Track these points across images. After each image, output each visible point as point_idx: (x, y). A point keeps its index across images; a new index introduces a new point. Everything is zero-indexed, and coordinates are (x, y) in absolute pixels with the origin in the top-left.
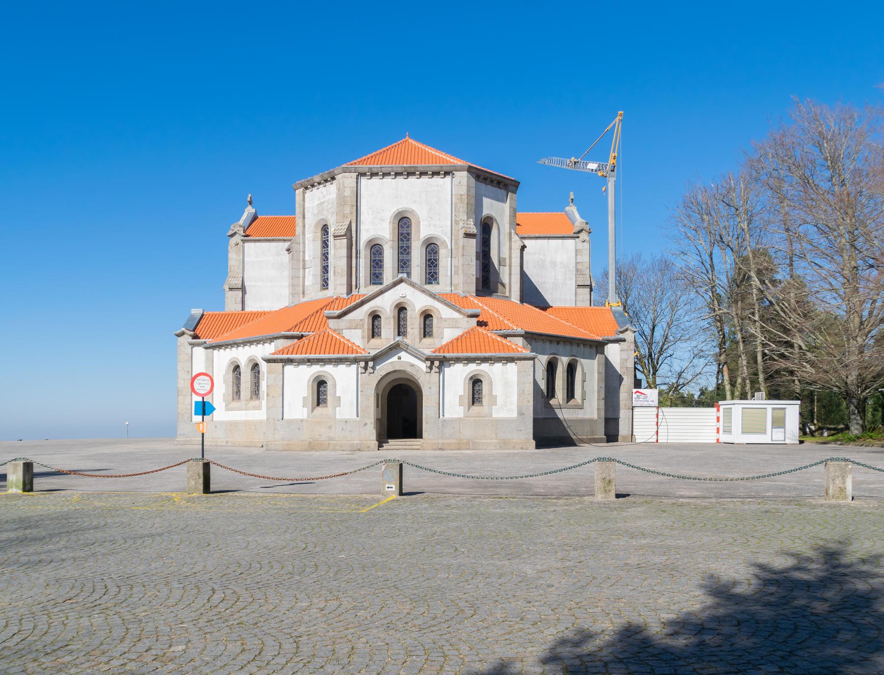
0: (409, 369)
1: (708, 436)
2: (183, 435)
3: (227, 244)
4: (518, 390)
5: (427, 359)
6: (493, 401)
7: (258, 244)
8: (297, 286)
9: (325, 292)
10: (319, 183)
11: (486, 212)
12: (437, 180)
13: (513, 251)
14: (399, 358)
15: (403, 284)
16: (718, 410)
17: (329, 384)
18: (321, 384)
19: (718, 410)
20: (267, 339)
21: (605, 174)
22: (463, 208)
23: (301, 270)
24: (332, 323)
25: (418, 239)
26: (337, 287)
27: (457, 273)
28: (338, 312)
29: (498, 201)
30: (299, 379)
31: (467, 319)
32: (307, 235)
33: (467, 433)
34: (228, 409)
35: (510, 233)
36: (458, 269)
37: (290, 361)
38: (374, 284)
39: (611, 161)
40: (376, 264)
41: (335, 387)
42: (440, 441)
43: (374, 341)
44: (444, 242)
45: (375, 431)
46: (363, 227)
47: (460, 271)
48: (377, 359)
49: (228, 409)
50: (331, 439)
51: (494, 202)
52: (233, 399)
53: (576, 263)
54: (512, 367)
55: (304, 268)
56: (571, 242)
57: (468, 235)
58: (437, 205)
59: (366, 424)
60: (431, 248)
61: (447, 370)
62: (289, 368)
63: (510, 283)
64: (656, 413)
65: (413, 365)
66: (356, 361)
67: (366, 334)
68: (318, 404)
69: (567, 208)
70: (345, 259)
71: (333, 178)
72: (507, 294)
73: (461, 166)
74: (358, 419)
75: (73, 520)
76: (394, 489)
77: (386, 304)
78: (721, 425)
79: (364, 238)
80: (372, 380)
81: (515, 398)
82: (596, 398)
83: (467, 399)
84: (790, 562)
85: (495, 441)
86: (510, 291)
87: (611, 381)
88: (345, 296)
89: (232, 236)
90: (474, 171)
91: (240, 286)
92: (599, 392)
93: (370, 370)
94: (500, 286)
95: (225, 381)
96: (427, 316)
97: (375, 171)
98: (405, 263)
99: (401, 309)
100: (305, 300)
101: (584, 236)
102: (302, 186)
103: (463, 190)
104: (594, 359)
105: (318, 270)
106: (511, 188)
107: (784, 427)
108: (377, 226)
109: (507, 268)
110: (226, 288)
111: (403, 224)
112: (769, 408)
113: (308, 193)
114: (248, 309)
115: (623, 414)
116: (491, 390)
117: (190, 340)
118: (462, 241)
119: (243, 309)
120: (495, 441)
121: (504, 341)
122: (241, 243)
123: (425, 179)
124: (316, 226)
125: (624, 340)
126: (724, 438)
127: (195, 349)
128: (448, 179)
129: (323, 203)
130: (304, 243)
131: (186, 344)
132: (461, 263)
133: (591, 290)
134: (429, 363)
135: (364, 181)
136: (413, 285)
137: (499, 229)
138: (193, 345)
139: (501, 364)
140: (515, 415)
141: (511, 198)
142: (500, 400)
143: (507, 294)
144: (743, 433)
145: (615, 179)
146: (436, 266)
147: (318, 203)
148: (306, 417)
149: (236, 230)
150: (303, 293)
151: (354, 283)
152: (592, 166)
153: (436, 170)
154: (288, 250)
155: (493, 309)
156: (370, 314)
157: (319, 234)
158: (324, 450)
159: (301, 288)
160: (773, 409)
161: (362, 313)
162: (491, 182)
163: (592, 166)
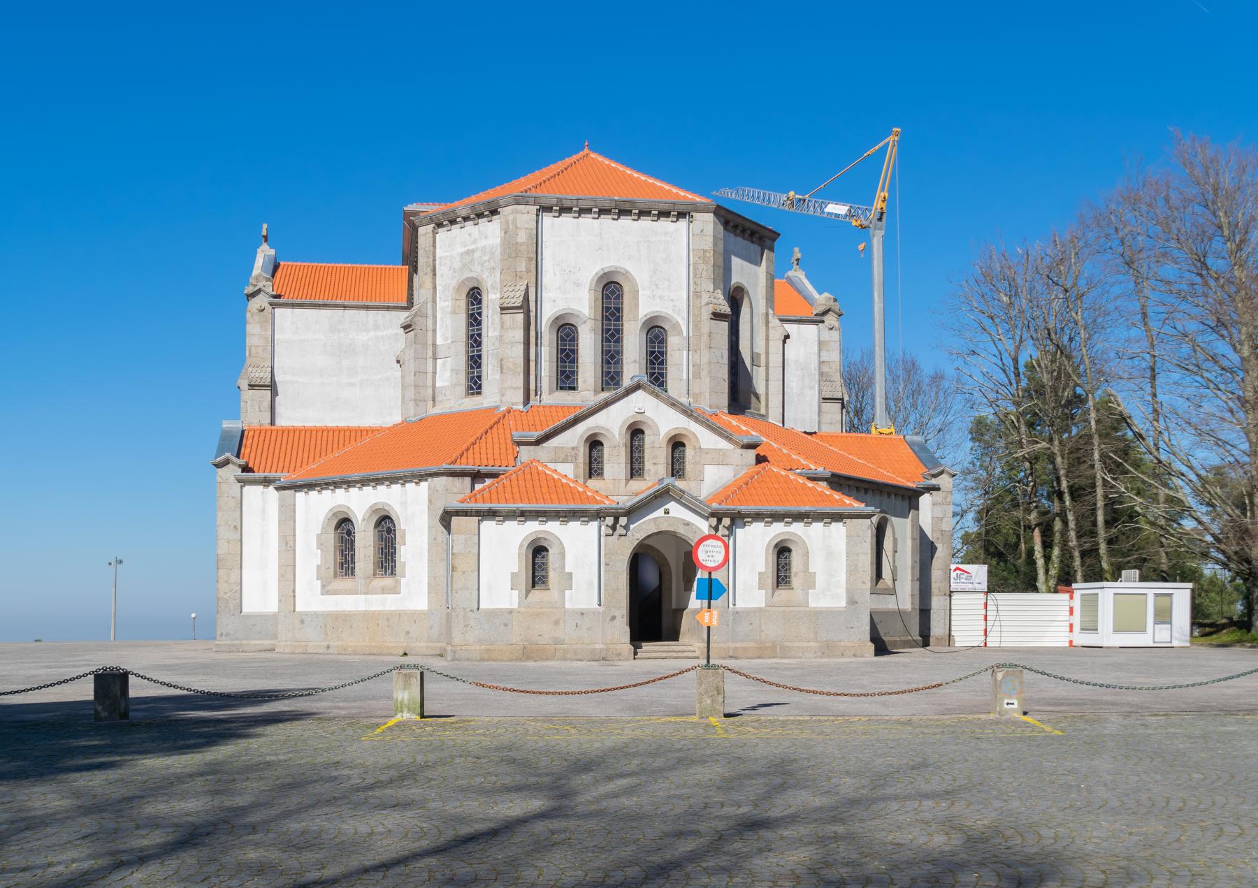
0: (681, 530)
1: (1056, 637)
2: (228, 635)
3: (244, 311)
4: (848, 566)
5: (713, 515)
6: (810, 582)
7: (298, 311)
8: (420, 385)
9: (476, 399)
10: (466, 219)
11: (735, 280)
12: (665, 224)
13: (771, 343)
14: (667, 512)
15: (640, 393)
16: (1071, 598)
17: (552, 554)
18: (538, 551)
19: (1071, 598)
20: (413, 476)
21: (865, 223)
22: (707, 271)
23: (430, 362)
24: (526, 453)
25: (636, 319)
26: (502, 389)
27: (697, 375)
28: (536, 434)
29: (750, 262)
30: (503, 544)
31: (740, 451)
32: (440, 304)
33: (771, 632)
34: (325, 591)
35: (767, 314)
36: (696, 366)
37: (492, 514)
38: (561, 388)
39: (878, 204)
41: (564, 558)
42: (731, 645)
44: (676, 326)
45: (628, 629)
46: (547, 295)
47: (704, 373)
48: (634, 512)
49: (325, 591)
50: (557, 641)
51: (746, 264)
52: (335, 576)
53: (821, 363)
54: (838, 529)
55: (435, 359)
56: (811, 329)
57: (717, 316)
58: (666, 264)
59: (614, 618)
60: (656, 334)
61: (739, 532)
62: (488, 526)
63: (767, 394)
64: (983, 601)
65: (687, 524)
66: (598, 515)
67: (581, 471)
68: (533, 586)
69: (790, 274)
70: (522, 347)
71: (494, 212)
72: (763, 412)
73: (704, 204)
74: (601, 609)
75: (225, 777)
76: (1016, 706)
77: (612, 422)
78: (1077, 619)
79: (549, 312)
80: (624, 548)
81: (842, 578)
82: (909, 578)
83: (770, 580)
84: (600, 874)
85: (814, 644)
86: (767, 406)
87: (926, 549)
88: (521, 407)
89: (253, 295)
90: (723, 213)
91: (268, 382)
92: (913, 568)
93: (620, 530)
94: (753, 399)
95: (320, 545)
96: (677, 444)
97: (567, 204)
98: (612, 357)
99: (636, 431)
100: (438, 410)
101: (831, 319)
102: (431, 220)
103: (707, 243)
104: (906, 517)
105: (461, 362)
106: (768, 242)
107: (1170, 623)
108: (569, 295)
109: (762, 370)
110: (244, 384)
111: (611, 292)
112: (1151, 593)
113: (442, 234)
114: (281, 422)
115: (937, 603)
116: (807, 565)
117: (238, 471)
118: (707, 324)
119: (273, 423)
120: (814, 644)
121: (810, 484)
122: (269, 308)
123: (645, 222)
124: (458, 289)
125: (937, 489)
126: (1081, 639)
127: (247, 489)
128: (683, 223)
129: (473, 251)
130: (435, 317)
131: (232, 479)
132: (705, 359)
133: (843, 406)
134: (714, 521)
135: (547, 219)
137: (751, 307)
138: (244, 482)
139: (802, 524)
140: (842, 603)
141: (768, 259)
142: (820, 580)
143: (763, 412)
144: (1115, 631)
145: (883, 232)
146: (662, 363)
147: (461, 252)
148: (515, 606)
149: (260, 285)
150: (434, 400)
151: (532, 387)
152: (841, 209)
153: (665, 208)
154: (407, 327)
155: (767, 436)
156: (587, 440)
157: (463, 303)
158: (547, 659)
159: (430, 392)
160: (1157, 595)
161: (574, 438)
162: (746, 232)
163: (841, 209)
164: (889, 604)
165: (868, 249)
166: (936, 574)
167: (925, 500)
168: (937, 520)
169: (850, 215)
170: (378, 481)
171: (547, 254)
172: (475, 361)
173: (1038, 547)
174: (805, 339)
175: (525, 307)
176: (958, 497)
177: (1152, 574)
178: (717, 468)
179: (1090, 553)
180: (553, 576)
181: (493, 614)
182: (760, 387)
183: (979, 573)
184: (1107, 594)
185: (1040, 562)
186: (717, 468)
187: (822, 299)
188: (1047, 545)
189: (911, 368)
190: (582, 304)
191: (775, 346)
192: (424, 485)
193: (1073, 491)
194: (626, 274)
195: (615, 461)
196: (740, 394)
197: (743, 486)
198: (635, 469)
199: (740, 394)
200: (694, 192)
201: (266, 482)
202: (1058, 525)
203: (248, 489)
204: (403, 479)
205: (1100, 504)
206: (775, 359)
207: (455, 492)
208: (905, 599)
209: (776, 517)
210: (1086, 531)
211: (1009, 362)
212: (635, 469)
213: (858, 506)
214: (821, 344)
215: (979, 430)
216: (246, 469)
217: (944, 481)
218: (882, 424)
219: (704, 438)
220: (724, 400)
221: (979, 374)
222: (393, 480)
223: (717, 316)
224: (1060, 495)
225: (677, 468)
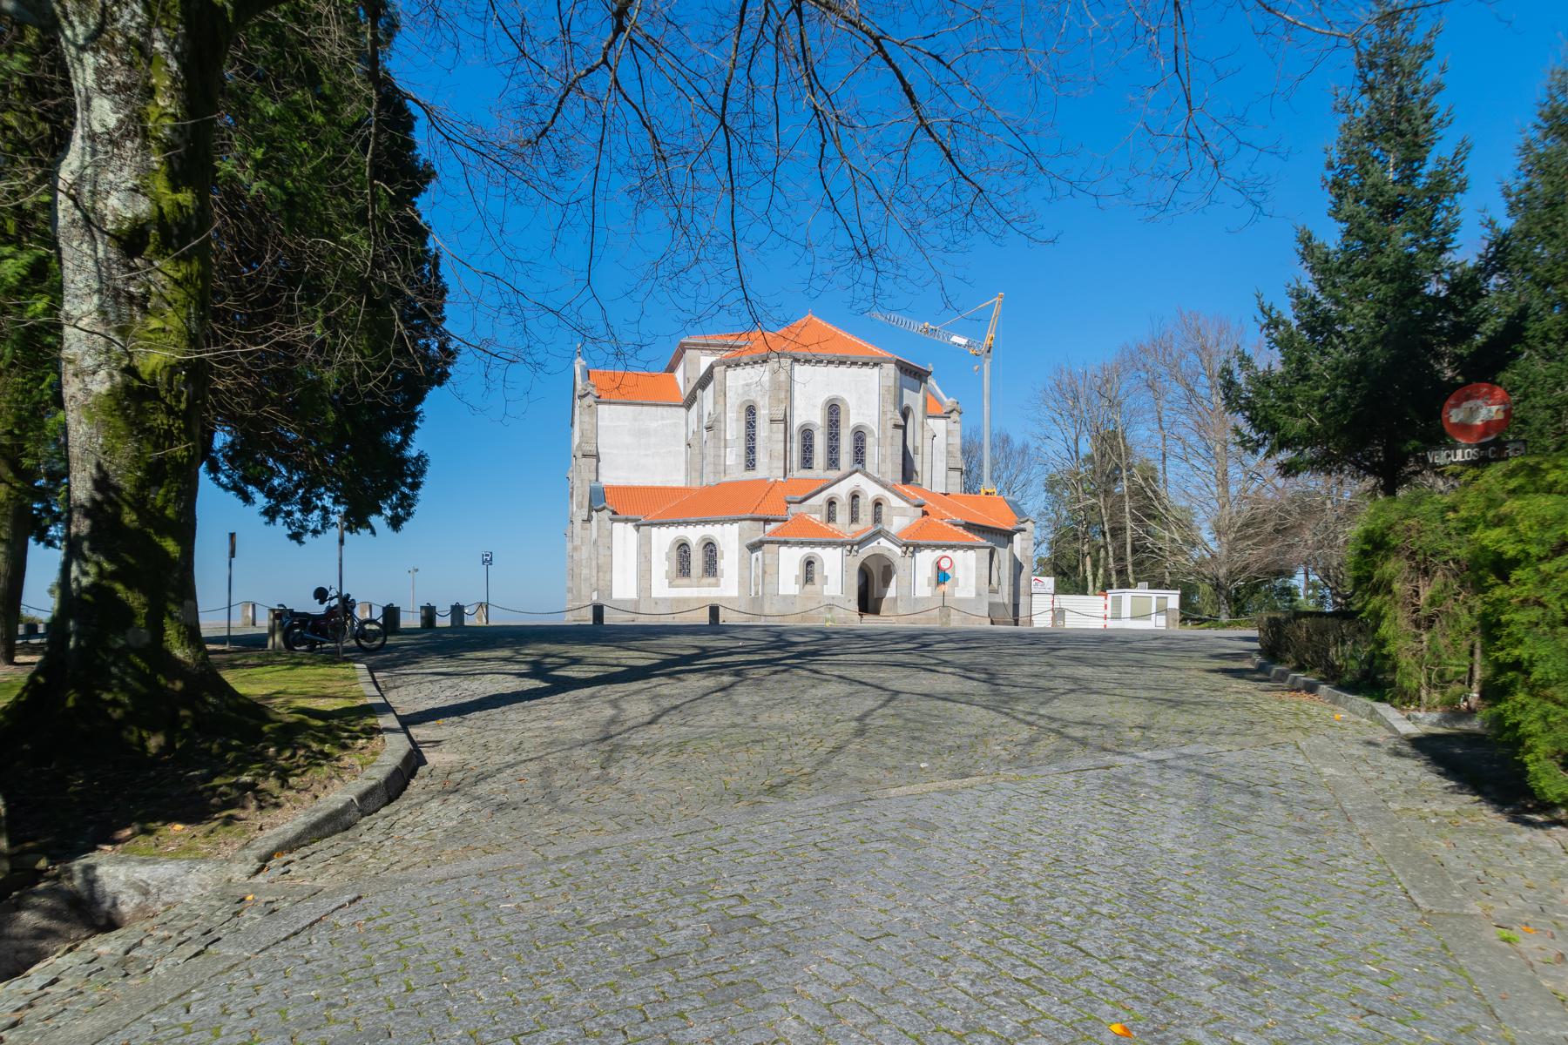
6: (956, 584)
7: (612, 407)
12: (865, 370)
22: (890, 399)
24: (793, 508)
27: (884, 461)
28: (799, 498)
34: (671, 585)
36: (882, 456)
37: (786, 543)
40: (807, 448)
43: (855, 527)
44: (872, 432)
48: (862, 543)
49: (671, 585)
54: (971, 553)
57: (896, 426)
58: (864, 394)
60: (859, 436)
62: (783, 550)
66: (843, 544)
77: (842, 491)
79: (797, 422)
80: (856, 563)
83: (802, 580)
87: (1017, 567)
95: (668, 558)
96: (878, 504)
99: (855, 497)
100: (727, 479)
101: (955, 416)
103: (891, 382)
108: (809, 412)
110: (750, 475)
111: (834, 411)
113: (730, 372)
115: (1023, 600)
118: (890, 431)
123: (854, 369)
128: (876, 370)
135: (797, 367)
136: (867, 475)
138: (613, 521)
161: (820, 500)
162: (913, 374)
164: (997, 599)
165: (981, 369)
166: (1023, 582)
167: (1017, 537)
168: (1024, 550)
169: (968, 346)
170: (706, 522)
171: (797, 388)
172: (751, 450)
173: (1089, 568)
174: (939, 426)
175: (785, 420)
176: (1037, 533)
177: (1157, 584)
178: (900, 517)
179: (1121, 572)
180: (817, 577)
181: (785, 597)
182: (918, 467)
183: (1049, 582)
184: (1127, 596)
185: (1090, 578)
186: (900, 517)
187: (949, 402)
188: (1095, 566)
189: (1006, 440)
190: (817, 418)
191: (928, 442)
192: (736, 526)
193: (1112, 530)
194: (842, 400)
195: (843, 515)
196: (908, 473)
197: (918, 529)
198: (854, 518)
199: (908, 473)
200: (882, 348)
201: (627, 521)
202: (1102, 553)
203: (616, 525)
204: (723, 522)
205: (1129, 540)
206: (927, 449)
207: (757, 532)
208: (1005, 596)
209: (938, 547)
210: (1120, 559)
211: (1071, 443)
212: (854, 518)
213: (983, 542)
214: (948, 432)
215: (1051, 486)
216: (614, 513)
217: (1028, 526)
218: (987, 485)
219: (895, 501)
220: (899, 476)
221: (1058, 446)
222: (716, 522)
223: (896, 426)
224: (1104, 534)
225: (877, 519)
